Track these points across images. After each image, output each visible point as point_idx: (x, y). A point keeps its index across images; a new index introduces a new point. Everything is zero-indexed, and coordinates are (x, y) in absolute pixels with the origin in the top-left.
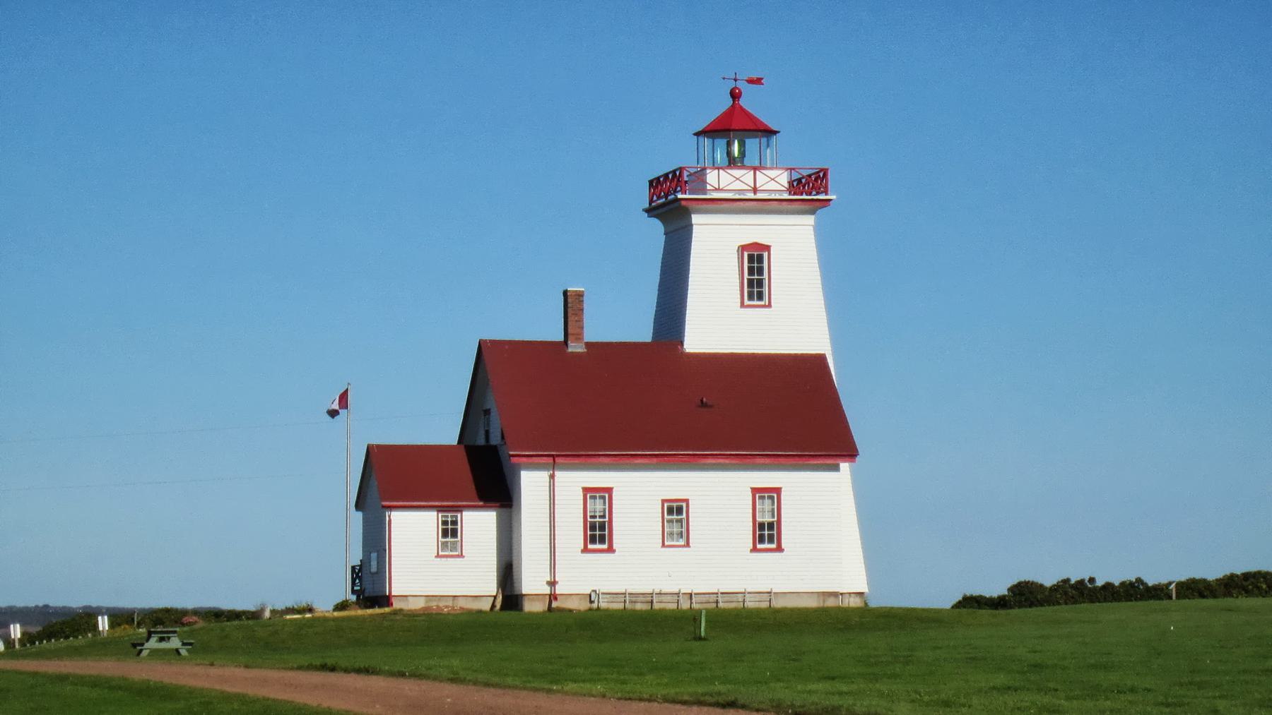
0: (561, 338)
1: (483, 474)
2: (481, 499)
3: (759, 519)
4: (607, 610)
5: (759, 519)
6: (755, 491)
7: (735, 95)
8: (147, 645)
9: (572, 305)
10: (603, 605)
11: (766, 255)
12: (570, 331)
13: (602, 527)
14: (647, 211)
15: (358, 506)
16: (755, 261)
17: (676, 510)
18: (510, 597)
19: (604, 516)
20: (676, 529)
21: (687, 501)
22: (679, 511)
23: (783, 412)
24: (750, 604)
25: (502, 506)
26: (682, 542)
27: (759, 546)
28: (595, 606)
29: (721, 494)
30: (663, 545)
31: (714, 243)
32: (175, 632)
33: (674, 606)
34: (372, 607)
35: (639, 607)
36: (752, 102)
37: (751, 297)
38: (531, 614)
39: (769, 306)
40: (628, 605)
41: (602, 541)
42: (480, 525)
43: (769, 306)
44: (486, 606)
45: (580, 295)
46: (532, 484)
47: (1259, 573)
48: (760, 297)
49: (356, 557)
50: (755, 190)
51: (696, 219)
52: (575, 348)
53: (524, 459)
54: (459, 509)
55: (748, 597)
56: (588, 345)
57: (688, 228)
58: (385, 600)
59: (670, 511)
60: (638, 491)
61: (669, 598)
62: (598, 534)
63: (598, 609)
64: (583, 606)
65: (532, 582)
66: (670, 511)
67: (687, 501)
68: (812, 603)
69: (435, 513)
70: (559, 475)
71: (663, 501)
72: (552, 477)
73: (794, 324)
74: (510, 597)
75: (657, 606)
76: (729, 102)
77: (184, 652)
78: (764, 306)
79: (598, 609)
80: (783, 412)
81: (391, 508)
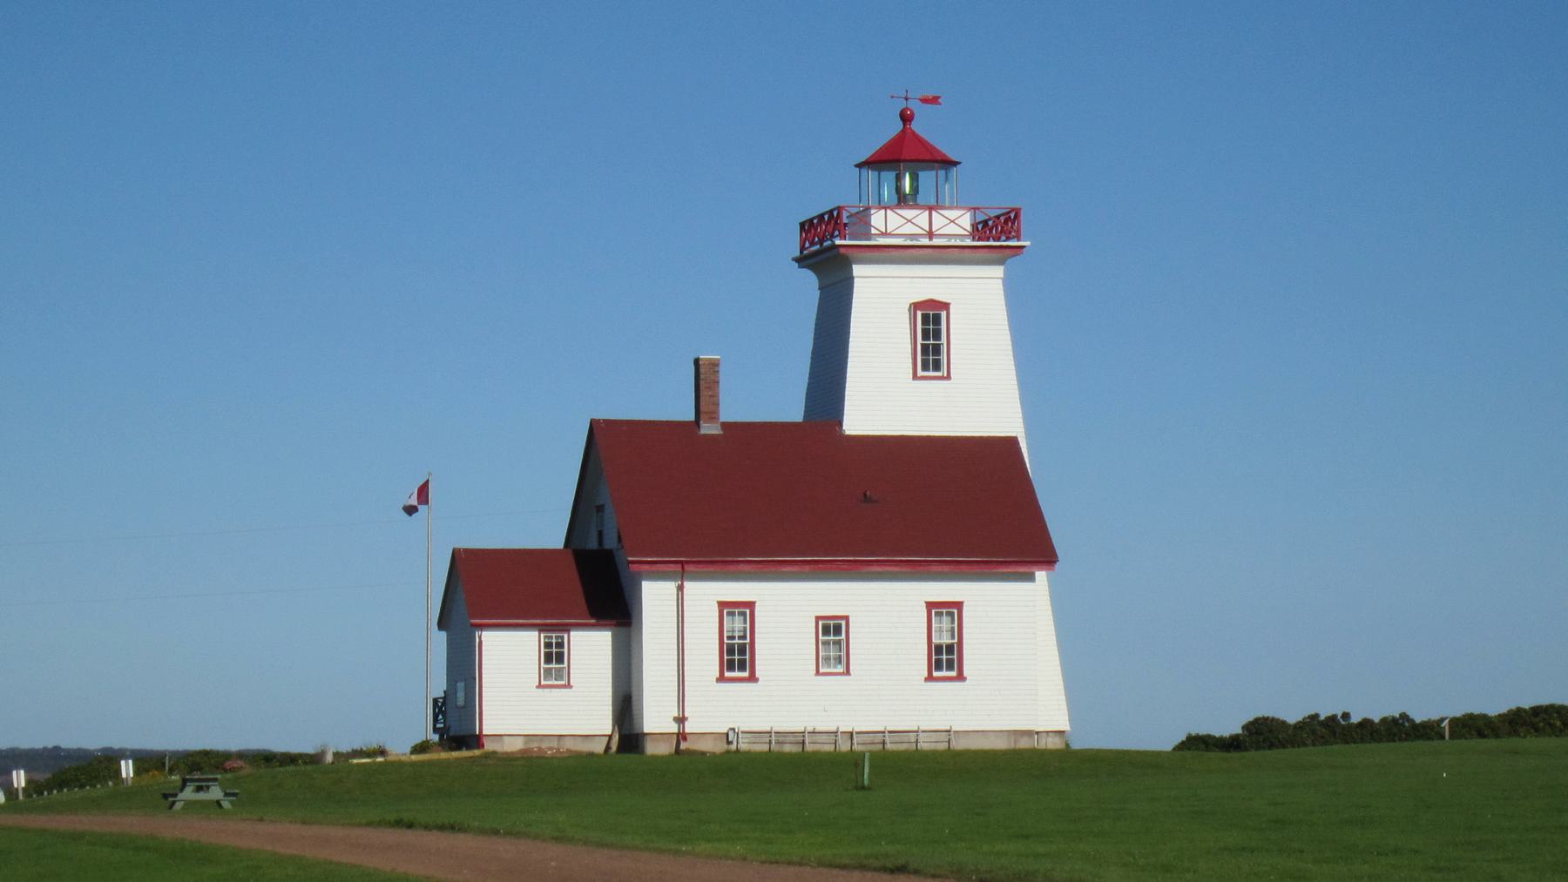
2: (593, 616)
3: (935, 640)
5: (935, 640)
6: (930, 605)
7: (906, 117)
8: (181, 796)
9: (704, 378)
10: (744, 747)
11: (944, 314)
13: (742, 650)
14: (797, 260)
15: (442, 625)
16: (930, 322)
17: (832, 629)
18: (629, 735)
19: (744, 637)
21: (847, 618)
22: (837, 630)
23: (962, 509)
25: (618, 625)
26: (840, 669)
27: (935, 674)
28: (733, 747)
29: (888, 610)
30: (818, 672)
31: (881, 300)
33: (830, 748)
34: (458, 748)
35: (787, 748)
37: (925, 367)
39: (948, 377)
40: (774, 747)
41: (742, 667)
42: (591, 648)
43: (948, 377)
44: (599, 747)
45: (714, 365)
48: (937, 367)
49: (439, 688)
50: (931, 235)
51: (858, 270)
52: (707, 429)
53: (646, 567)
54: (567, 628)
55: (922, 737)
56: (725, 426)
58: (475, 740)
59: (826, 631)
60: (787, 606)
61: (824, 738)
62: (737, 659)
64: (719, 747)
65: (656, 718)
67: (847, 618)
68: (1001, 744)
70: (689, 586)
72: (680, 588)
73: (978, 399)
74: (629, 735)
75: (809, 748)
76: (900, 126)
77: (226, 804)
80: (962, 509)
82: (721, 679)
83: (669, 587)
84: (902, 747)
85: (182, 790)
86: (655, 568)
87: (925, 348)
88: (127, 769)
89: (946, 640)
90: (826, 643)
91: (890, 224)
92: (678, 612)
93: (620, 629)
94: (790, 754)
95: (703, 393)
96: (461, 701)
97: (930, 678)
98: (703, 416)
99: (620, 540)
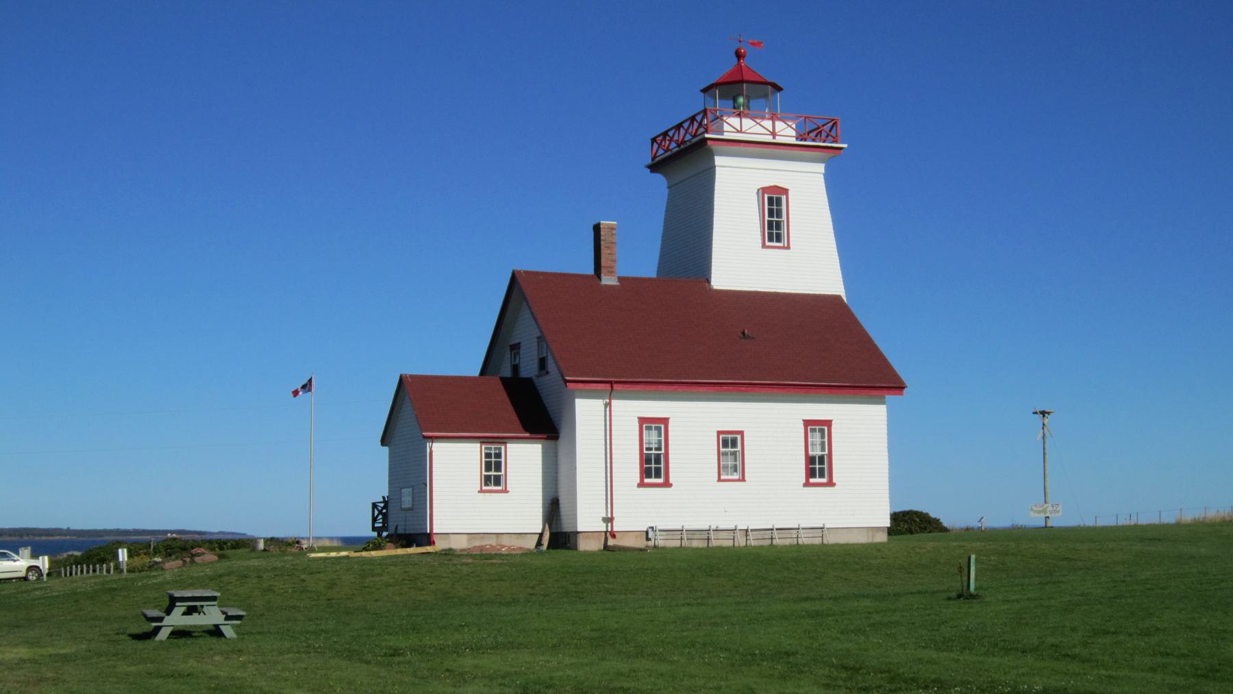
0: (589, 270)
1: (523, 402)
3: (811, 453)
5: (811, 453)
7: (739, 55)
8: (168, 620)
10: (661, 543)
11: (784, 198)
12: (603, 263)
13: (658, 461)
15: (384, 441)
16: (774, 203)
17: (730, 442)
18: (560, 536)
19: (659, 449)
21: (741, 433)
22: (734, 444)
23: (810, 350)
24: (805, 540)
25: (548, 438)
26: (736, 476)
27: (647, 481)
28: (651, 543)
29: (774, 425)
30: (719, 480)
31: (736, 185)
32: (213, 599)
33: (729, 543)
34: (409, 545)
35: (695, 544)
36: (758, 64)
37: (771, 240)
38: (587, 554)
39: (788, 248)
40: (685, 543)
41: (658, 475)
42: (524, 458)
43: (788, 248)
44: (531, 544)
46: (587, 412)
47: (916, 513)
48: (779, 239)
49: (381, 490)
50: (774, 134)
51: (719, 160)
52: (608, 280)
53: (581, 386)
54: (503, 441)
55: (712, 536)
56: (620, 279)
58: (427, 539)
59: (725, 444)
60: (695, 421)
61: (724, 535)
62: (654, 467)
63: (655, 547)
64: (640, 543)
65: (587, 518)
66: (725, 444)
67: (741, 433)
68: (862, 539)
70: (616, 403)
71: (719, 433)
73: (810, 264)
74: (560, 536)
75: (714, 543)
77: (228, 631)
78: (783, 248)
81: (433, 439)
82: (642, 485)
84: (787, 542)
85: (169, 611)
86: (588, 386)
87: (770, 223)
88: (123, 554)
89: (816, 452)
91: (733, 127)
93: (550, 443)
95: (604, 251)
96: (407, 501)
97: (807, 484)
98: (603, 270)
99: (542, 363)
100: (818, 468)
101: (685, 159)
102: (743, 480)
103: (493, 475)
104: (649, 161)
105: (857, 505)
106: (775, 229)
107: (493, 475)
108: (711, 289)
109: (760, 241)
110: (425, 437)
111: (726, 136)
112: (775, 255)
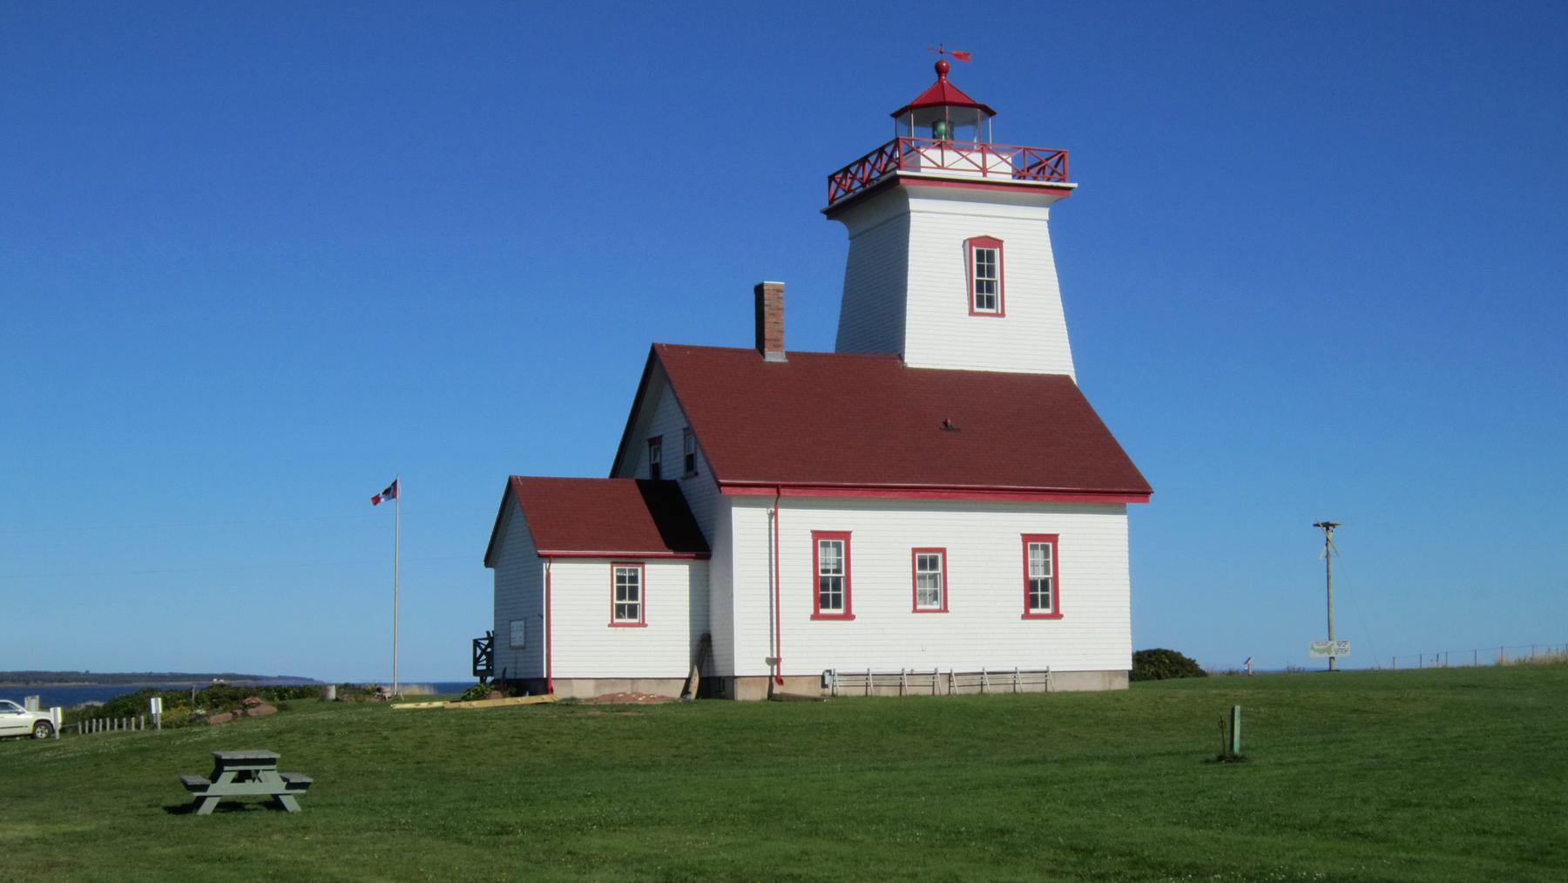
0: (751, 344)
1: (665, 511)
2: (670, 546)
3: (1031, 576)
4: (845, 697)
5: (1031, 576)
7: (940, 70)
8: (214, 789)
10: (840, 691)
11: (997, 252)
13: (837, 586)
15: (488, 561)
16: (984, 258)
17: (928, 562)
18: (712, 682)
19: (838, 571)
20: (929, 589)
21: (943, 551)
23: (1030, 446)
24: (1023, 687)
26: (936, 606)
28: (828, 691)
29: (984, 541)
30: (915, 610)
31: (936, 235)
32: (271, 761)
35: (884, 692)
36: (964, 82)
37: (980, 305)
38: (747, 705)
39: (1003, 315)
40: (872, 691)
41: (837, 604)
42: (667, 582)
44: (675, 692)
46: (747, 524)
47: (1165, 652)
48: (990, 304)
49: (484, 624)
51: (914, 204)
52: (773, 356)
53: (739, 490)
54: (640, 560)
55: (987, 678)
57: (904, 216)
60: (883, 536)
62: (831, 594)
63: (833, 695)
64: (815, 691)
65: (747, 659)
67: (943, 551)
68: (1096, 686)
69: (608, 566)
70: (783, 513)
72: (774, 515)
73: (1030, 336)
74: (712, 682)
75: (908, 691)
77: (291, 803)
79: (833, 695)
81: (551, 558)
82: (816, 616)
83: (758, 515)
84: (1001, 689)
85: (214, 778)
86: (748, 491)
88: (156, 705)
89: (1038, 575)
90: (923, 577)
92: (767, 541)
93: (698, 562)
94: (887, 698)
96: (518, 638)
97: (1026, 616)
98: (767, 343)
100: (1040, 596)
101: (871, 202)
102: (945, 610)
103: (628, 604)
104: (826, 205)
105: (1091, 642)
106: (985, 292)
107: (628, 604)
108: (905, 368)
109: (911, 604)
110: (540, 556)
111: (924, 173)
112: (986, 324)
